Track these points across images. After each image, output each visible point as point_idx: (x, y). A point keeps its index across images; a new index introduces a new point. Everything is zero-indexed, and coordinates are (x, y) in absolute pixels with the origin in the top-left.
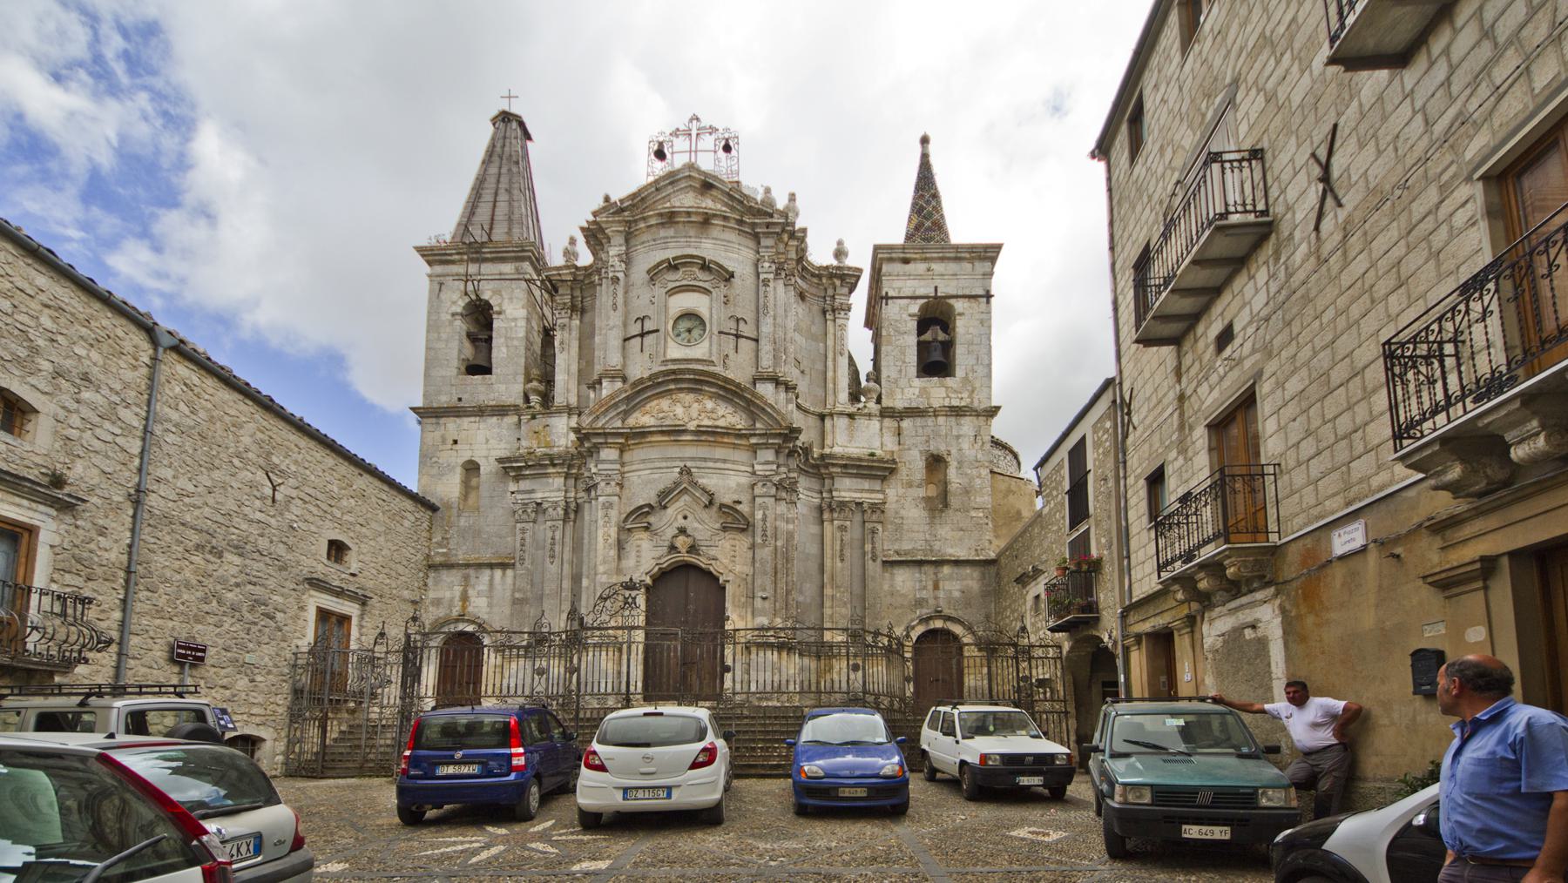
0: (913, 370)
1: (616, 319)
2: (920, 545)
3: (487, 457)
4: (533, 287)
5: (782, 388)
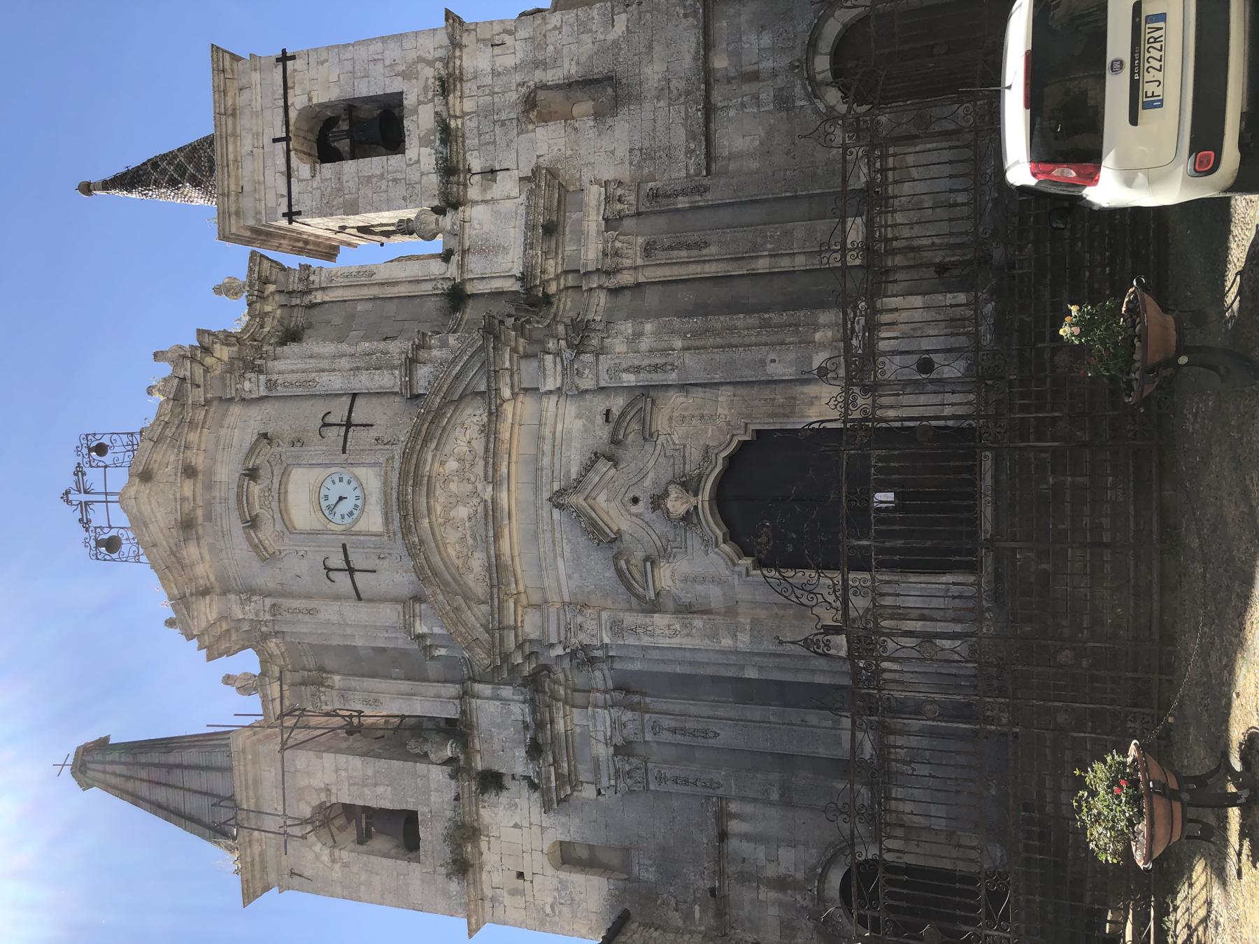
0: (394, 160)
1: (329, 612)
2: (677, 114)
3: (543, 829)
4: (291, 742)
5: (423, 354)
